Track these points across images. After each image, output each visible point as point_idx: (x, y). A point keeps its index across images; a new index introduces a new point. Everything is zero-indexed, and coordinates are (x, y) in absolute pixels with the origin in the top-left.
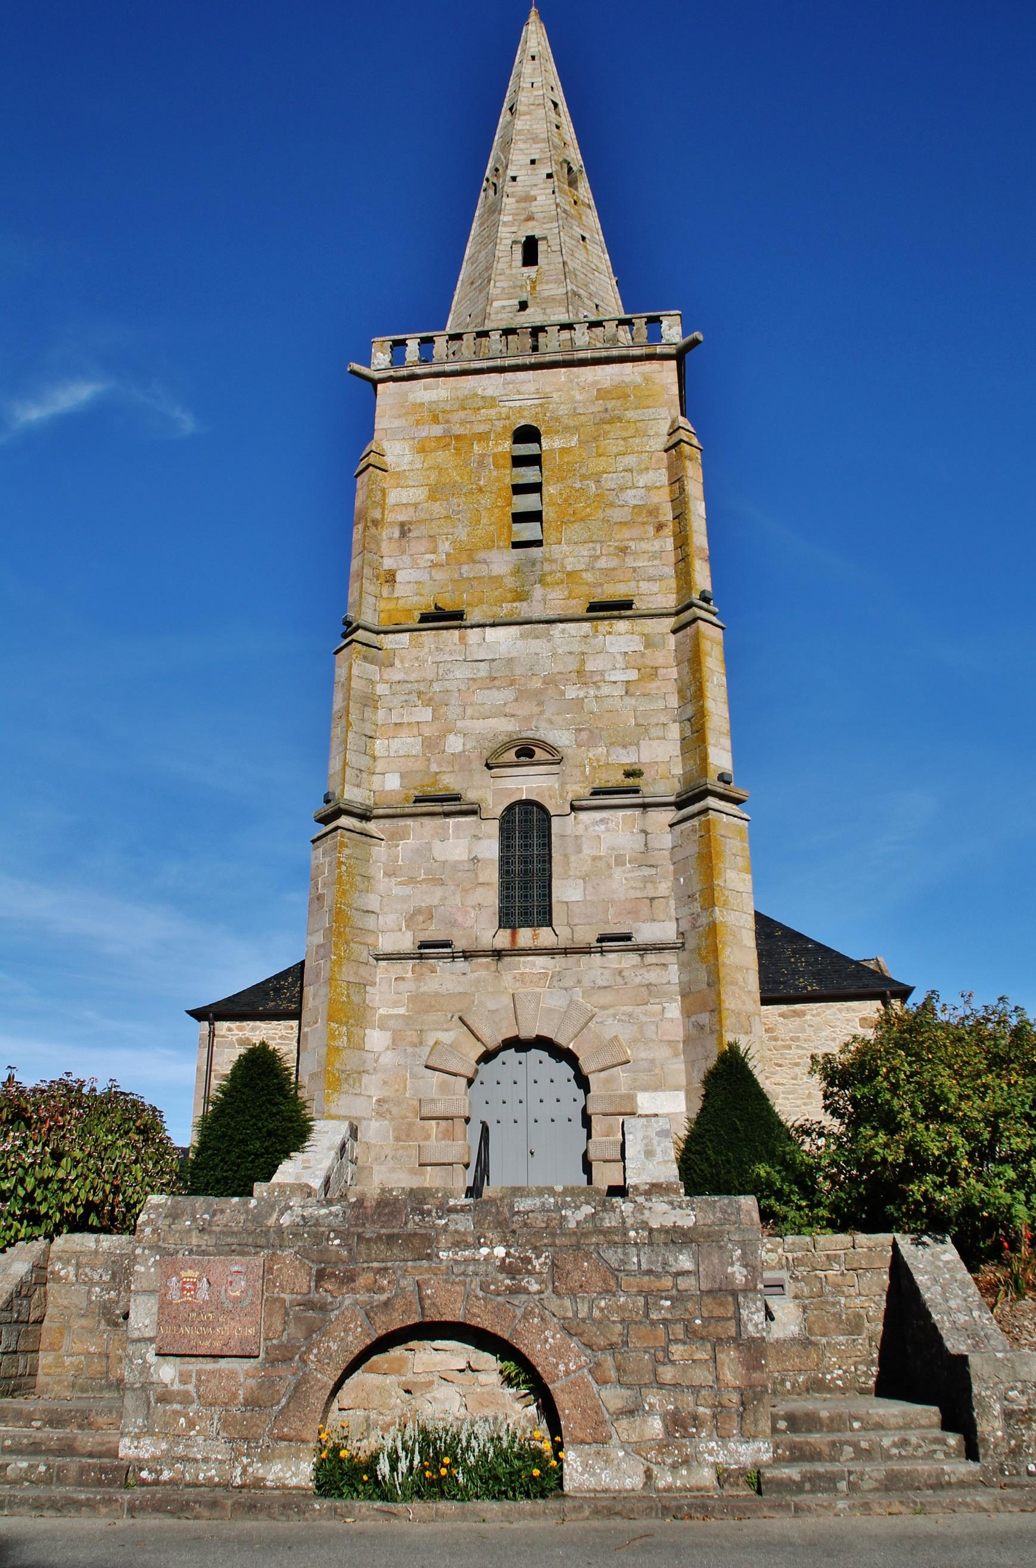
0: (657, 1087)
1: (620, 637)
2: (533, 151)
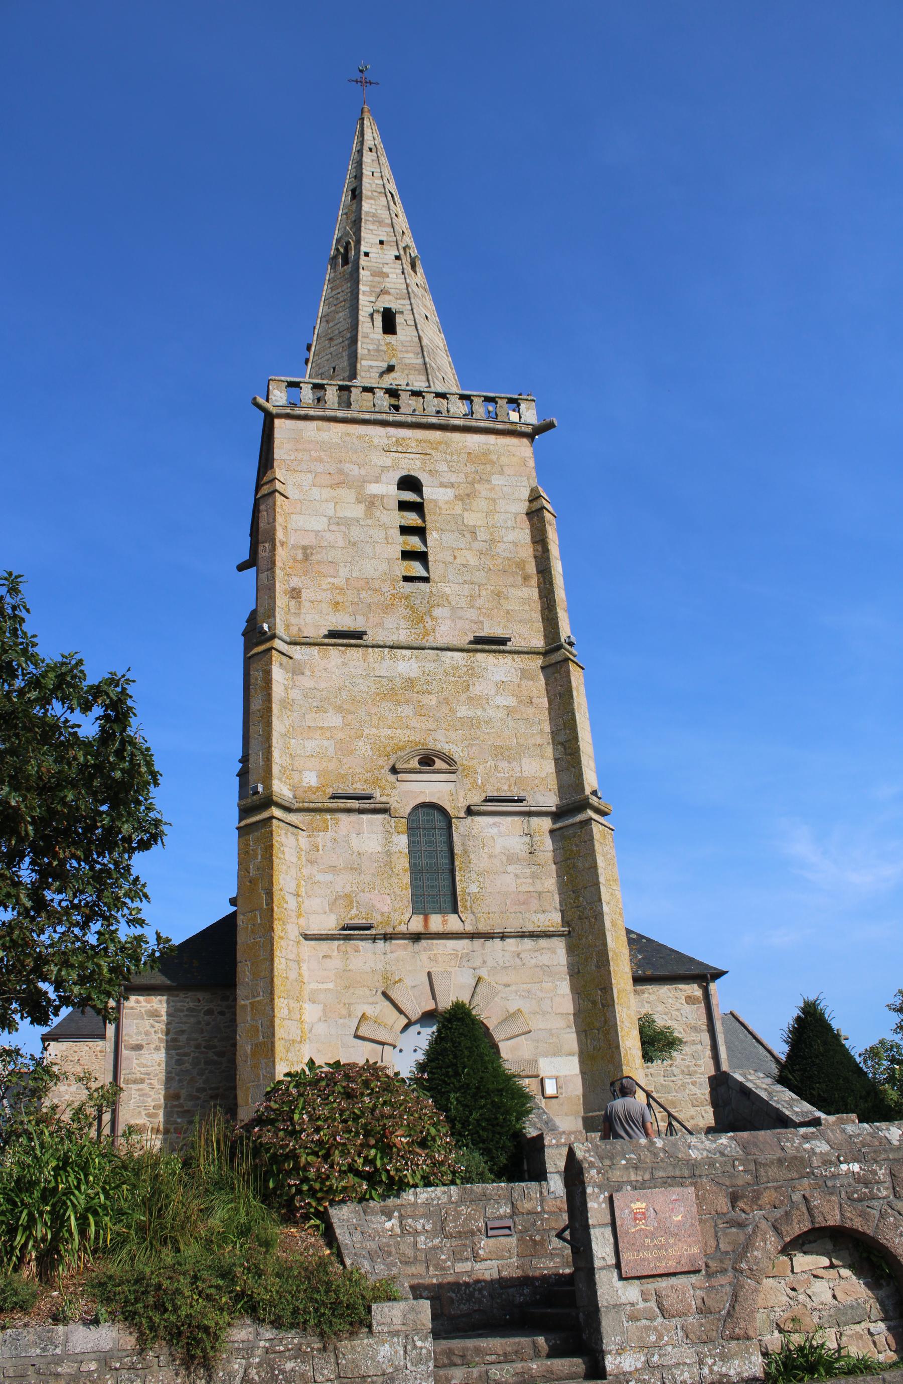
0: (556, 1052)
1: (496, 668)
2: (381, 233)
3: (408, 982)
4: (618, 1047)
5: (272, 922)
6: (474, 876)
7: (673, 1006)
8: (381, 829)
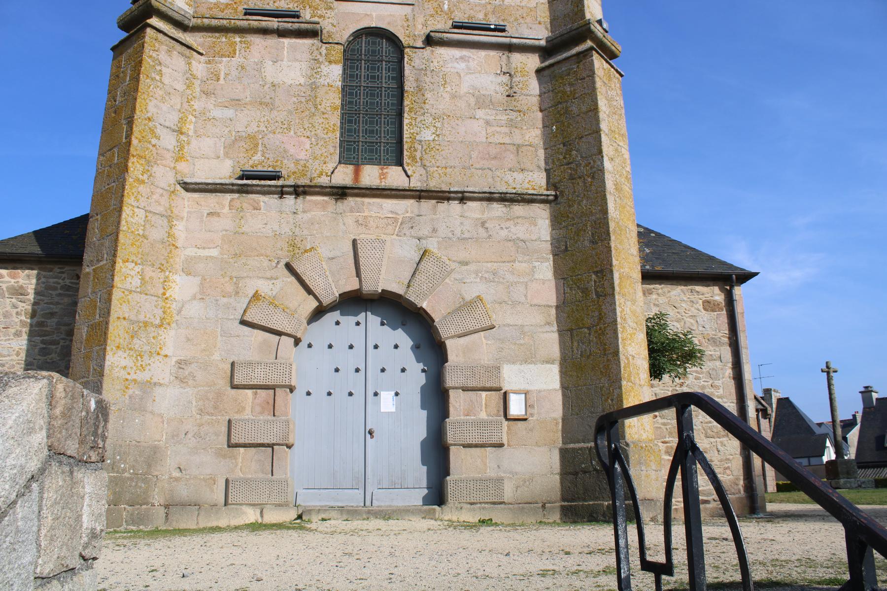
0: (529, 358)
3: (324, 251)
4: (616, 353)
5: (127, 159)
6: (429, 120)
7: (689, 310)
8: (306, 56)
